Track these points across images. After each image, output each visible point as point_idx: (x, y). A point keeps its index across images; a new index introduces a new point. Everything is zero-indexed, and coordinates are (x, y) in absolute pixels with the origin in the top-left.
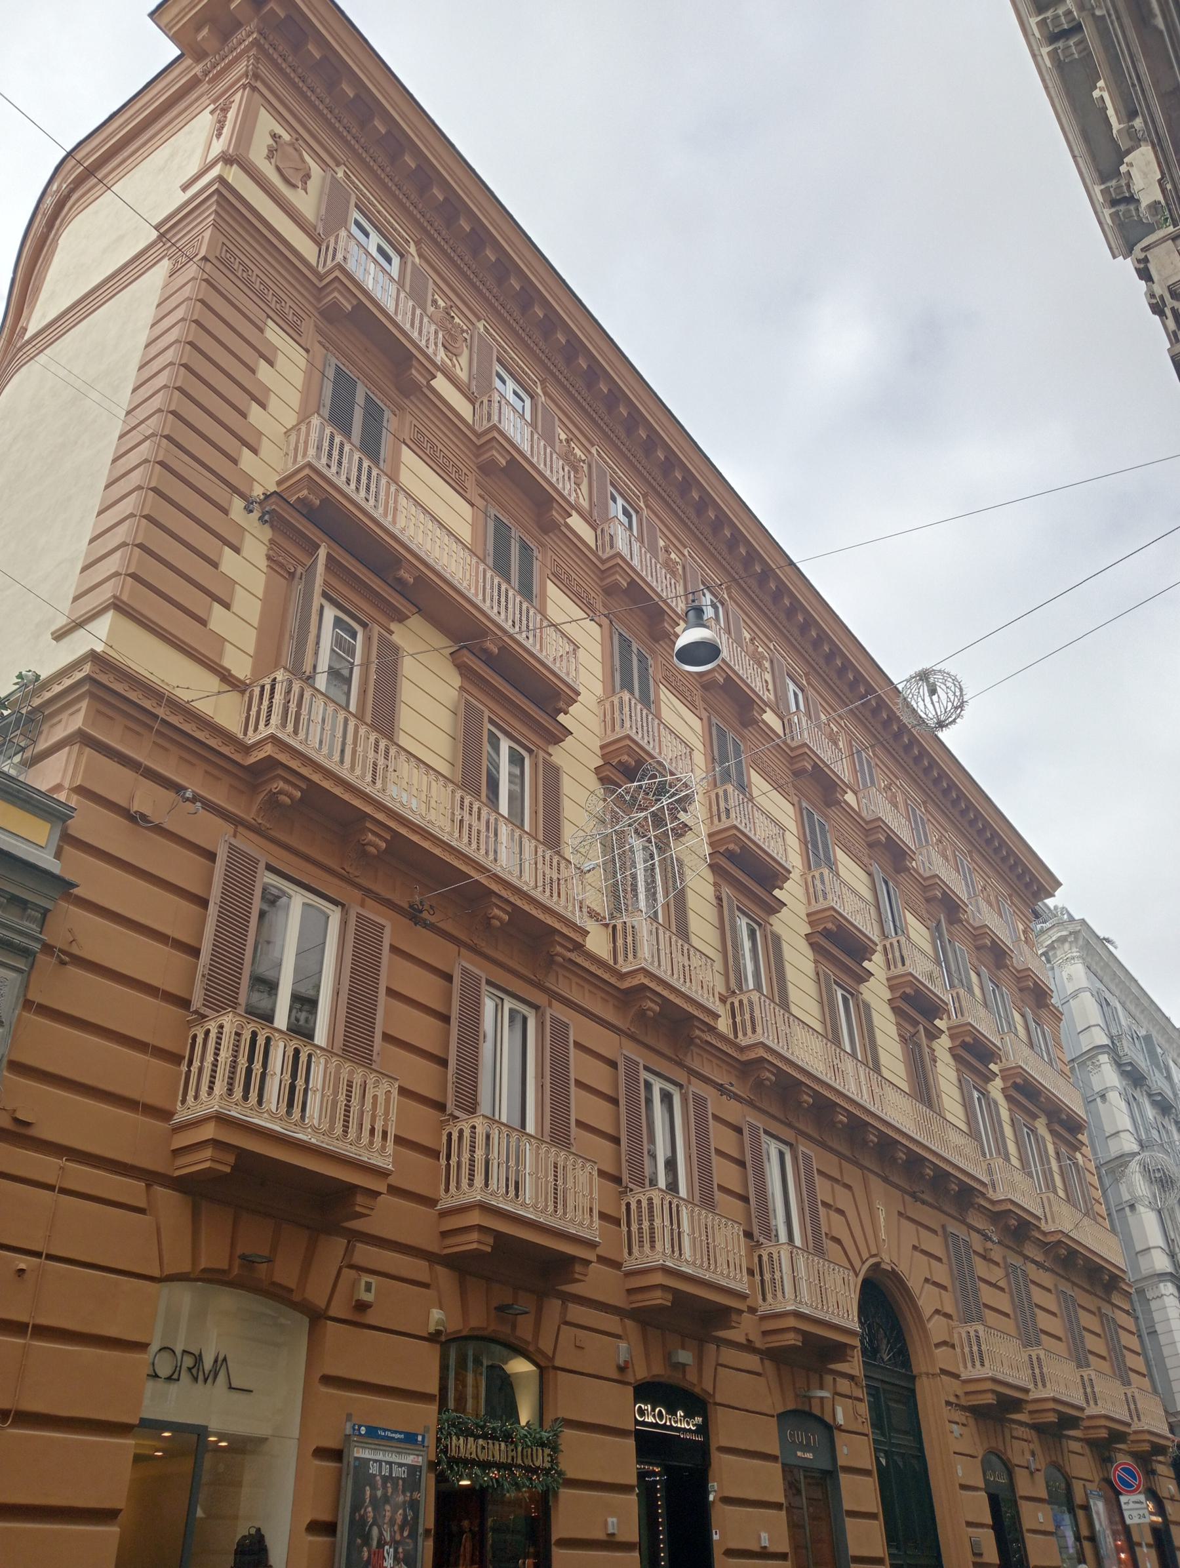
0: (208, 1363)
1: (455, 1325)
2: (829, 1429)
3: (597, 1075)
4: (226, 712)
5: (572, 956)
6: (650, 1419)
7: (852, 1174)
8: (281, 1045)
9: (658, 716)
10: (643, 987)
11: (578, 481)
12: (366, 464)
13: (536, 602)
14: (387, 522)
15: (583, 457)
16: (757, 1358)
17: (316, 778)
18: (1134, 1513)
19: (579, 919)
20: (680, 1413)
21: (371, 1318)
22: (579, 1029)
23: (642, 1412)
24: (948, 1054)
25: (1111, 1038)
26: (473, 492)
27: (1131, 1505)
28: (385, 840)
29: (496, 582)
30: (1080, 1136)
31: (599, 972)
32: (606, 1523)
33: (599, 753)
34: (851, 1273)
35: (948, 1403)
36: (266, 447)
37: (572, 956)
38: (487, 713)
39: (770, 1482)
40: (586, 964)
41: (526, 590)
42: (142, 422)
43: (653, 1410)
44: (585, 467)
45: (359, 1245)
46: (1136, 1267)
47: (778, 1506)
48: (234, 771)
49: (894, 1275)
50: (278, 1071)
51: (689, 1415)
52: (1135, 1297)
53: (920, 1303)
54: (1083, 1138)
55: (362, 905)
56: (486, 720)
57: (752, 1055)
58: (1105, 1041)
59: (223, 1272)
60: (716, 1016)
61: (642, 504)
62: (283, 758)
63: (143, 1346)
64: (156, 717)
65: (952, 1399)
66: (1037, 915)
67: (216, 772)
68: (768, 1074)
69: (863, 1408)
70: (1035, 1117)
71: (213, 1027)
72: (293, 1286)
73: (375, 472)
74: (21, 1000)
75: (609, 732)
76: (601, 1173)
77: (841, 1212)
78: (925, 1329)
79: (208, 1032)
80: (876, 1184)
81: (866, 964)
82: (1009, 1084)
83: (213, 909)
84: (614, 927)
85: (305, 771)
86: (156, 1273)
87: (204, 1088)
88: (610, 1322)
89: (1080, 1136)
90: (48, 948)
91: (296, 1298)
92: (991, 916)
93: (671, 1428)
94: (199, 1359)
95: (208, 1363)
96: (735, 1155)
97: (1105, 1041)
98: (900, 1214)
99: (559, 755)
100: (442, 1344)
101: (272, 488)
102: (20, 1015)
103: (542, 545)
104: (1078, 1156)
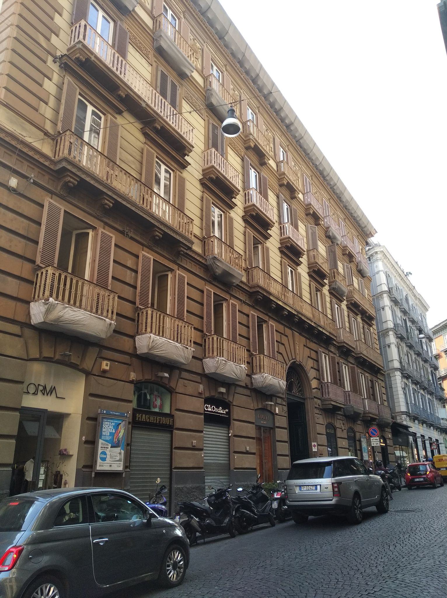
0: (48, 389)
1: (140, 378)
2: (273, 414)
3: (196, 295)
4: (46, 149)
5: (188, 252)
6: (210, 410)
7: (288, 332)
9: (227, 159)
10: (64, 169)
11: (197, 57)
12: (120, 58)
13: (177, 108)
14: (122, 76)
15: (200, 47)
17: (83, 176)
18: (375, 443)
20: (221, 408)
21: (107, 375)
23: (207, 407)
26: (153, 59)
27: (374, 440)
28: (112, 203)
29: (160, 99)
30: (373, 322)
31: (198, 258)
32: (192, 443)
33: (201, 172)
34: (285, 364)
36: (62, 34)
37: (188, 252)
38: (212, 201)
39: (250, 430)
40: (193, 255)
41: (173, 104)
42: (7, 19)
43: (211, 407)
44: (201, 51)
46: (388, 366)
47: (253, 438)
48: (51, 172)
49: (300, 366)
51: (224, 409)
52: (386, 376)
53: (309, 375)
54: (374, 322)
55: (104, 229)
56: (78, 93)
58: (386, 289)
59: (52, 358)
60: (193, 243)
61: (224, 69)
62: (69, 167)
63: (22, 383)
64: (16, 148)
65: (317, 406)
66: (367, 244)
67: (32, 166)
69: (285, 408)
70: (357, 315)
71: (44, 271)
72: (79, 364)
73: (124, 62)
75: (206, 164)
76: (195, 328)
77: (283, 344)
78: (310, 383)
79: (42, 273)
81: (300, 259)
82: (311, 270)
83: (43, 227)
84: (205, 242)
86: (26, 358)
87: (41, 293)
88: (198, 378)
89: (373, 322)
91: (81, 368)
92: (355, 247)
93: (217, 413)
94: (45, 388)
95: (48, 389)
97: (386, 289)
98: (304, 345)
100: (135, 384)
101: (65, 52)
103: (182, 84)
104: (371, 328)
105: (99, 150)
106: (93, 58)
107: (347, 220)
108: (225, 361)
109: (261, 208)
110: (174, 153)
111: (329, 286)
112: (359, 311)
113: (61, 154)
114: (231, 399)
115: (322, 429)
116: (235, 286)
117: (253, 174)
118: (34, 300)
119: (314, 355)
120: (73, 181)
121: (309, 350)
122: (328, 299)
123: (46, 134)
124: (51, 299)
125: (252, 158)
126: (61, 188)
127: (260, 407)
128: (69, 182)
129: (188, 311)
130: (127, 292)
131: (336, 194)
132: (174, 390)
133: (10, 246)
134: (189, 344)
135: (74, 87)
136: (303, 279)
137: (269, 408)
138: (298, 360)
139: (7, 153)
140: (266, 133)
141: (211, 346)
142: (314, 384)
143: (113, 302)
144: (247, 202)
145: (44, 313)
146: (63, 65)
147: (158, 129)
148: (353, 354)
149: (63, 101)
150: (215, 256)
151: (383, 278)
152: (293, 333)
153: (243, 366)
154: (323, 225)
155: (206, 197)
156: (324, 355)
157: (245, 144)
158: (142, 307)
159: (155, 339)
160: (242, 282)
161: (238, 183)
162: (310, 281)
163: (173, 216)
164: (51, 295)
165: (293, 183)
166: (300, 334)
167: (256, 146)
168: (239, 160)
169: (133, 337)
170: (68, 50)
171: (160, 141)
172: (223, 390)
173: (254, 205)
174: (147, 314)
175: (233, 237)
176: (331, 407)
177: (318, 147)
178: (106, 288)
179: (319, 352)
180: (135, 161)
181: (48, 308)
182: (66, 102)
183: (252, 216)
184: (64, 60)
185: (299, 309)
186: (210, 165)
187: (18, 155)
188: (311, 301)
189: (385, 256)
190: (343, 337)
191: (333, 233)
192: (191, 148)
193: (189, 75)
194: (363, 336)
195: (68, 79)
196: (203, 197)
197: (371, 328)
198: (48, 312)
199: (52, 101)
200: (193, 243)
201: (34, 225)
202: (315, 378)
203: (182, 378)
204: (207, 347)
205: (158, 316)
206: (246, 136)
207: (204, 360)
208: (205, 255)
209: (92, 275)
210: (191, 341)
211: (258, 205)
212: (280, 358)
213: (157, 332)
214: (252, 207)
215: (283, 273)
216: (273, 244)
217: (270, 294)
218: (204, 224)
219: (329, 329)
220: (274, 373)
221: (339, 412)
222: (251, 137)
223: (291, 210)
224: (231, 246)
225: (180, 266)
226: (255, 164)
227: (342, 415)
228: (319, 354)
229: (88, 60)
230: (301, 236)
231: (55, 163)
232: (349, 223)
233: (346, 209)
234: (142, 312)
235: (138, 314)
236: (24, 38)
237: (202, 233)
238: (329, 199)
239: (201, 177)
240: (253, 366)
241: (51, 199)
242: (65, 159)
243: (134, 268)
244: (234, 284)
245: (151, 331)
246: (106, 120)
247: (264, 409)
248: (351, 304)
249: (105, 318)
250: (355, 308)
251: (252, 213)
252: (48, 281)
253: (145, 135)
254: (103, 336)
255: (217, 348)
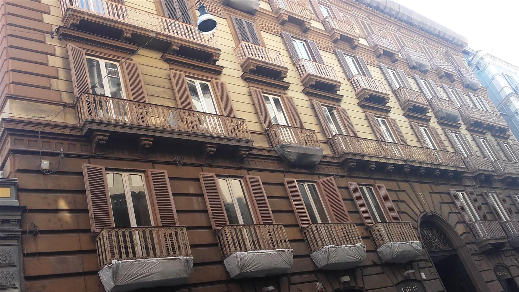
2: (421, 281)
3: (277, 192)
4: (70, 120)
7: (404, 186)
8: (137, 232)
10: (91, 131)
16: (380, 268)
17: (112, 129)
19: (250, 137)
22: (259, 177)
24: (403, 117)
25: (514, 89)
30: (428, 114)
31: (266, 154)
33: (301, 84)
35: (472, 254)
36: (53, 10)
38: (184, 74)
45: (194, 288)
48: (79, 139)
49: (434, 216)
50: (247, 237)
55: (249, 174)
57: (477, 173)
60: (252, 142)
61: (329, 4)
62: (95, 127)
64: (37, 132)
65: (474, 252)
68: (352, 163)
69: (434, 270)
73: (124, 8)
74: (22, 255)
76: (357, 225)
80: (416, 185)
81: (388, 105)
82: (406, 110)
83: (89, 194)
84: (268, 134)
85: (106, 129)
88: (313, 277)
90: (24, 233)
96: (450, 201)
99: (343, 105)
102: (23, 260)
103: (254, 20)
104: (509, 141)
105: (218, 114)
106: (86, 17)
107: (429, 41)
108: (335, 247)
109: (371, 89)
110: (202, 65)
111: (436, 117)
112: (485, 128)
113: (83, 119)
114: (360, 284)
115: (490, 275)
116: (319, 164)
117: (349, 60)
118: (101, 268)
119: (446, 198)
120: (103, 138)
121: (438, 195)
122: (440, 132)
123: (65, 105)
124: (114, 262)
125: (292, 30)
126: (96, 150)
127: (400, 279)
128: (100, 140)
129: (273, 212)
130: (199, 219)
131: (405, 21)
132: (363, 288)
133: (62, 226)
134: (285, 246)
135: (79, 51)
136: (399, 123)
137: (412, 277)
138: (429, 211)
139: (31, 140)
140: (345, 18)
141: (313, 237)
142: (460, 229)
143: (184, 237)
144: (357, 90)
145: (112, 278)
146: (61, 37)
147: (177, 50)
148: (495, 178)
149: (72, 68)
150: (282, 144)
151: (502, 82)
152: (410, 185)
153: (358, 244)
154: (403, 59)
155: (316, 103)
156: (490, 195)
157: (278, 21)
158: (220, 228)
159: (242, 256)
160: (324, 157)
161: (284, 61)
162: (410, 121)
163: (296, 134)
164: (113, 256)
165: (347, 34)
166: (420, 182)
167: (290, 17)
168: (278, 39)
169: (221, 262)
170: (63, 21)
171: (184, 60)
172: (346, 279)
173: (364, 89)
174: (312, 230)
175: (299, 116)
176: (491, 247)
177: (403, 7)
178: (174, 226)
179: (512, 196)
180: (166, 90)
181: (113, 271)
182: (75, 68)
183: (312, 86)
184: (61, 31)
185: (434, 162)
186: (245, 58)
187: (41, 137)
188: (375, 134)
189: (494, 58)
190: (478, 164)
191: (416, 62)
192: (219, 52)
193: (258, 8)
194: (501, 154)
195: (70, 45)
196: (312, 105)
197: (509, 141)
198: (115, 275)
199: (62, 74)
200: (252, 142)
201: (80, 196)
202: (458, 222)
203: (293, 284)
204: (309, 240)
205: (326, 228)
206: (276, 13)
207: (312, 255)
208: (273, 147)
209: (510, 217)
210: (359, 238)
211: (367, 87)
212: (404, 217)
213: (342, 242)
214: (308, 78)
215: (374, 128)
216: (349, 103)
217: (363, 155)
218: (261, 117)
219: (452, 164)
220: (403, 237)
221: (505, 248)
222: (281, 11)
223: (358, 62)
224: (405, 144)
225: (249, 169)
226: (298, 34)
227: (510, 250)
228: (485, 196)
229: (82, 21)
230: (377, 81)
231: (80, 129)
232: (433, 43)
233: (423, 30)
234: (308, 230)
235: (218, 236)
236: (17, 31)
237: (262, 127)
238: (399, 30)
239: (303, 88)
240: (374, 239)
241: (90, 163)
242: (88, 121)
243: (199, 192)
244: (317, 163)
245: (236, 249)
246: (121, 65)
247: (407, 281)
248: (472, 125)
249: (179, 257)
250: (477, 127)
251: (409, 107)
252: (106, 244)
253: (167, 61)
254: (184, 275)
255: (112, 247)
